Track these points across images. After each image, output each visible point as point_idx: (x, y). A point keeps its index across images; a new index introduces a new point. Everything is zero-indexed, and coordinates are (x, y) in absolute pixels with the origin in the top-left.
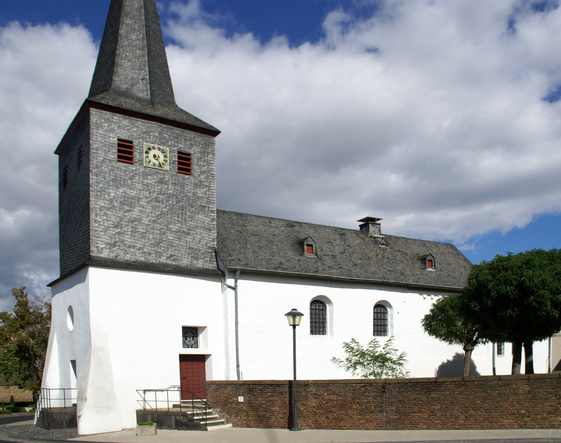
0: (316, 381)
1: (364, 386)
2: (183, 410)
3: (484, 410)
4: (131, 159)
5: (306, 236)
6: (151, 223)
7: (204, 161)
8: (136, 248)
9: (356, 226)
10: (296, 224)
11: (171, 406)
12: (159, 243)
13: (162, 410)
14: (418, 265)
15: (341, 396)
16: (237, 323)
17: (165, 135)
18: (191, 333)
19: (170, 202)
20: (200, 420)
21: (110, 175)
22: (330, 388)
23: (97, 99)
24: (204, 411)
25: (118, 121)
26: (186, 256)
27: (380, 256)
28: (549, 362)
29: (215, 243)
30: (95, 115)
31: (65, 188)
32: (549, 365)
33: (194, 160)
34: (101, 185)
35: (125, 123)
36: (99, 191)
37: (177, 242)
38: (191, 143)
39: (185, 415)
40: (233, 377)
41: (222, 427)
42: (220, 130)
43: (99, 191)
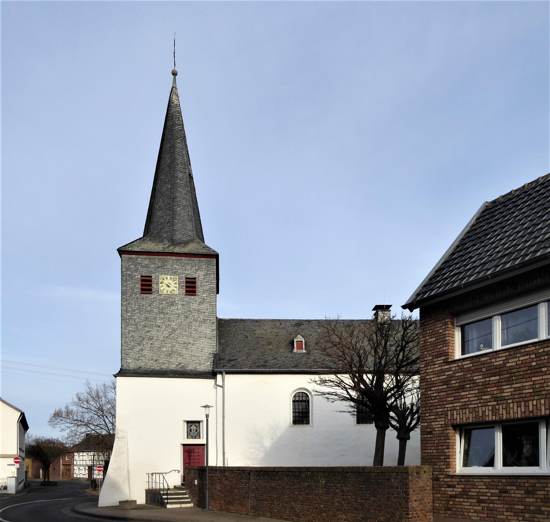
4: (151, 290)
10: (304, 322)
12: (170, 355)
16: (223, 417)
17: (176, 266)
18: (193, 426)
19: (180, 320)
33: (198, 284)
34: (129, 314)
36: (128, 319)
38: (200, 272)
40: (220, 464)
43: (128, 319)
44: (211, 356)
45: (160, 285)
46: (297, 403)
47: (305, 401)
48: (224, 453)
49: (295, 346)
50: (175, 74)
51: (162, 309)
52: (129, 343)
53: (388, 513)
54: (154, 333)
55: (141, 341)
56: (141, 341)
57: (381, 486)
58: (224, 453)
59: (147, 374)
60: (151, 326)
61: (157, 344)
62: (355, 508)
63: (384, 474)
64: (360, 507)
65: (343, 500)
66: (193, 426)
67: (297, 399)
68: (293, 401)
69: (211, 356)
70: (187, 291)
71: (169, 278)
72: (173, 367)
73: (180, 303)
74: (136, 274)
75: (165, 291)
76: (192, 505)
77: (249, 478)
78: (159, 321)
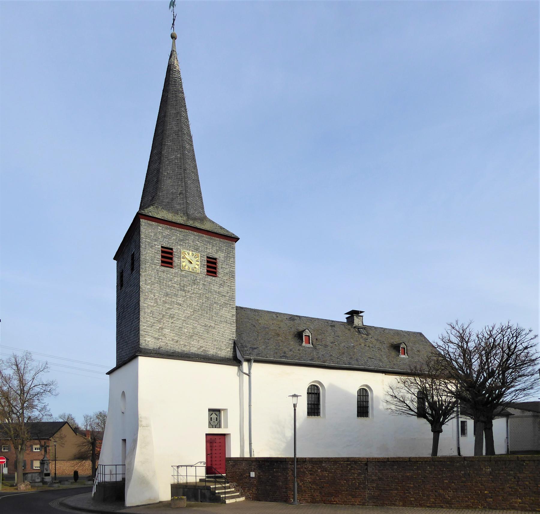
0: (312, 458)
1: (350, 465)
2: (208, 484)
3: (452, 489)
4: (171, 264)
6: (185, 319)
9: (343, 319)
10: (296, 318)
11: (198, 480)
12: (192, 336)
13: (191, 484)
14: (393, 353)
15: (331, 473)
16: (250, 406)
19: (201, 301)
21: (155, 278)
22: (323, 465)
23: (146, 212)
25: (161, 231)
27: (363, 345)
28: (508, 443)
29: (234, 336)
30: (145, 226)
32: (508, 446)
33: (219, 265)
35: (167, 233)
37: (206, 335)
40: (247, 455)
41: (238, 500)
42: (237, 234)
44: (231, 342)
45: (182, 260)
46: (310, 395)
47: (316, 394)
49: (304, 340)
50: (173, 37)
51: (184, 286)
52: (148, 319)
55: (161, 319)
56: (161, 319)
61: (179, 323)
68: (308, 393)
69: (231, 342)
70: (208, 271)
72: (194, 350)
73: (201, 282)
74: (156, 243)
75: (187, 267)
76: (242, 499)
77: (367, 469)
78: (180, 299)
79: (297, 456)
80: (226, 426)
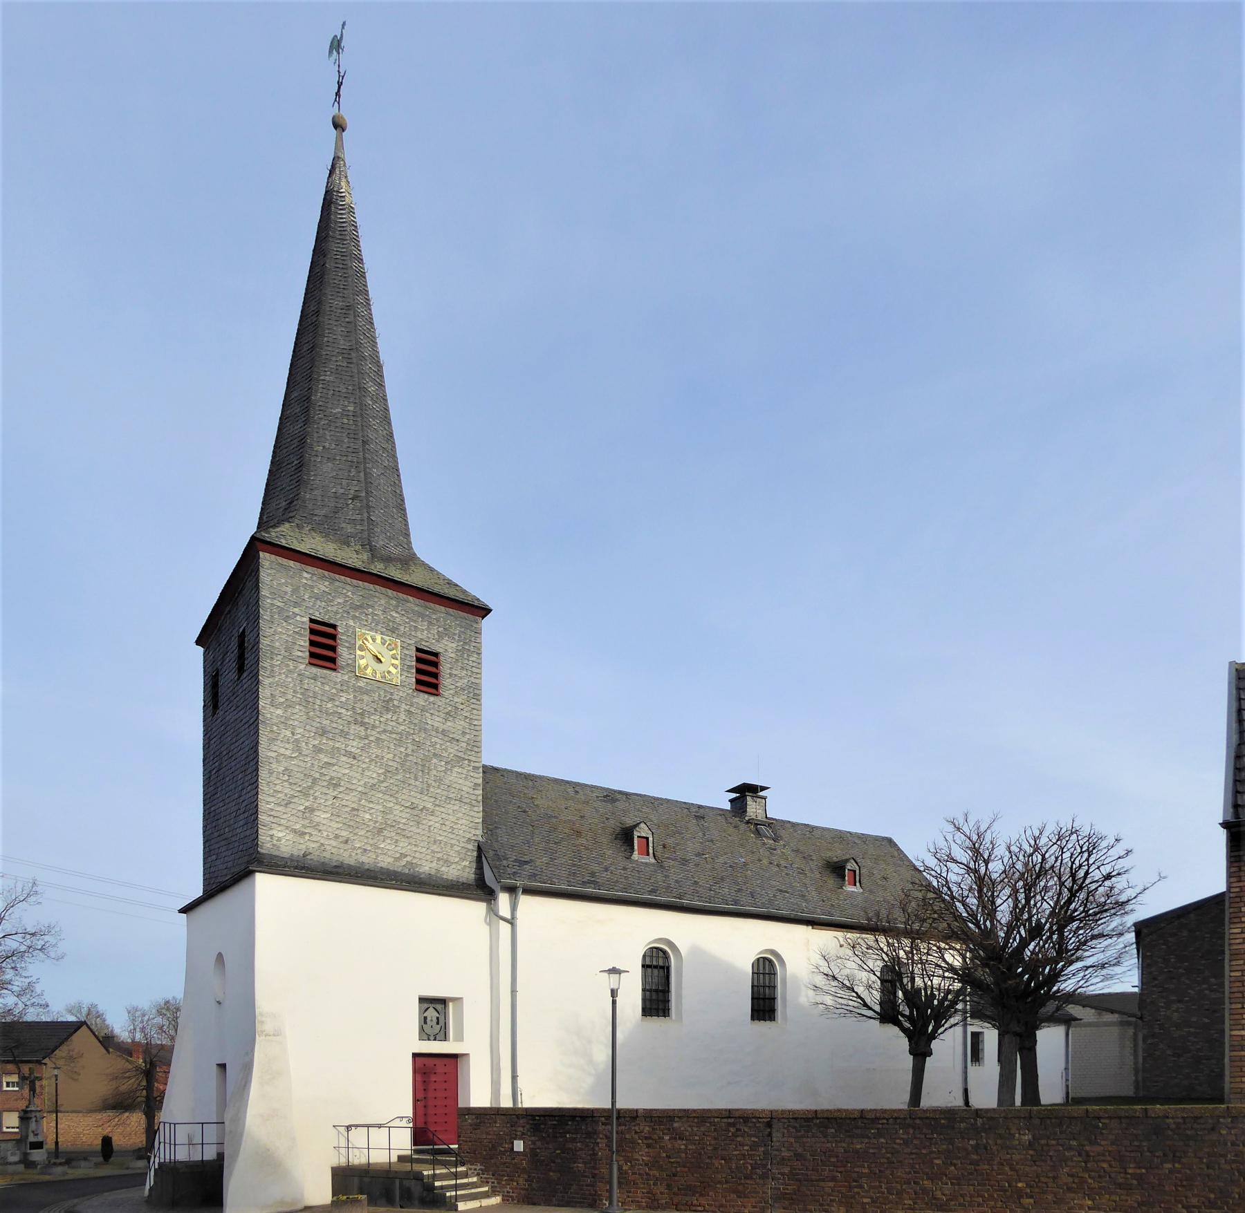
0: (651, 1110)
1: (733, 1125)
2: (417, 1167)
4: (333, 660)
5: (638, 820)
7: (462, 668)
8: (341, 839)
9: (723, 802)
10: (619, 796)
11: (394, 1159)
12: (380, 831)
14: (831, 881)
16: (514, 992)
19: (402, 749)
20: (466, 1175)
22: (676, 1125)
23: (272, 535)
24: (453, 1170)
25: (310, 583)
26: (428, 857)
29: (479, 832)
31: (214, 714)
32: (1067, 1086)
33: (445, 669)
36: (276, 725)
38: (434, 629)
39: (418, 1177)
40: (506, 1103)
42: (491, 606)
43: (276, 725)
44: (470, 847)
46: (649, 970)
47: (662, 967)
48: (514, 1078)
50: (338, 125)
51: (362, 714)
52: (278, 788)
53: (1212, 1191)
54: (342, 769)
56: (310, 788)
57: (1191, 1143)
58: (514, 1078)
59: (331, 873)
60: (334, 752)
61: (350, 800)
62: (1120, 1185)
63: (1202, 1121)
64: (1135, 1182)
65: (1086, 1169)
66: (431, 1010)
67: (648, 963)
69: (470, 847)
70: (418, 682)
71: (379, 640)
72: (385, 862)
74: (296, 610)
75: (369, 671)
76: (496, 1200)
77: (770, 1134)
79: (619, 1106)
80: (460, 1038)
